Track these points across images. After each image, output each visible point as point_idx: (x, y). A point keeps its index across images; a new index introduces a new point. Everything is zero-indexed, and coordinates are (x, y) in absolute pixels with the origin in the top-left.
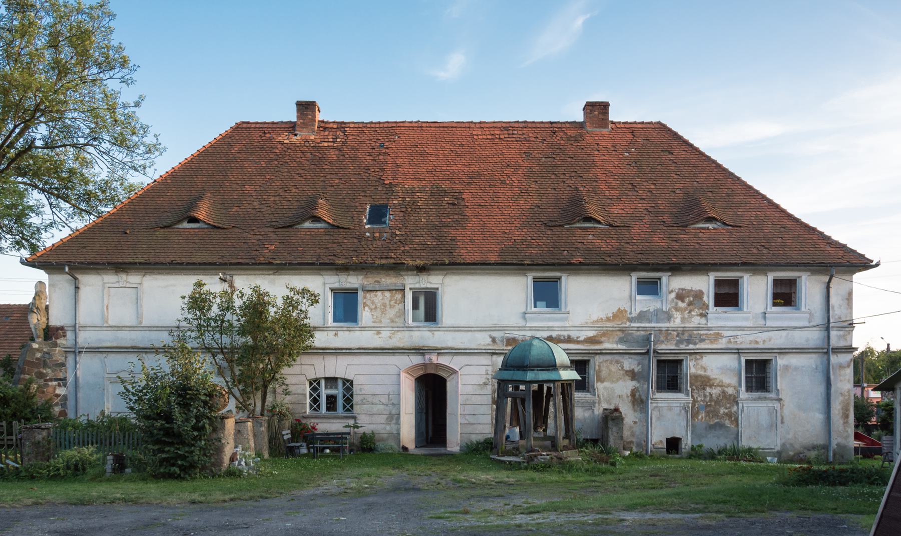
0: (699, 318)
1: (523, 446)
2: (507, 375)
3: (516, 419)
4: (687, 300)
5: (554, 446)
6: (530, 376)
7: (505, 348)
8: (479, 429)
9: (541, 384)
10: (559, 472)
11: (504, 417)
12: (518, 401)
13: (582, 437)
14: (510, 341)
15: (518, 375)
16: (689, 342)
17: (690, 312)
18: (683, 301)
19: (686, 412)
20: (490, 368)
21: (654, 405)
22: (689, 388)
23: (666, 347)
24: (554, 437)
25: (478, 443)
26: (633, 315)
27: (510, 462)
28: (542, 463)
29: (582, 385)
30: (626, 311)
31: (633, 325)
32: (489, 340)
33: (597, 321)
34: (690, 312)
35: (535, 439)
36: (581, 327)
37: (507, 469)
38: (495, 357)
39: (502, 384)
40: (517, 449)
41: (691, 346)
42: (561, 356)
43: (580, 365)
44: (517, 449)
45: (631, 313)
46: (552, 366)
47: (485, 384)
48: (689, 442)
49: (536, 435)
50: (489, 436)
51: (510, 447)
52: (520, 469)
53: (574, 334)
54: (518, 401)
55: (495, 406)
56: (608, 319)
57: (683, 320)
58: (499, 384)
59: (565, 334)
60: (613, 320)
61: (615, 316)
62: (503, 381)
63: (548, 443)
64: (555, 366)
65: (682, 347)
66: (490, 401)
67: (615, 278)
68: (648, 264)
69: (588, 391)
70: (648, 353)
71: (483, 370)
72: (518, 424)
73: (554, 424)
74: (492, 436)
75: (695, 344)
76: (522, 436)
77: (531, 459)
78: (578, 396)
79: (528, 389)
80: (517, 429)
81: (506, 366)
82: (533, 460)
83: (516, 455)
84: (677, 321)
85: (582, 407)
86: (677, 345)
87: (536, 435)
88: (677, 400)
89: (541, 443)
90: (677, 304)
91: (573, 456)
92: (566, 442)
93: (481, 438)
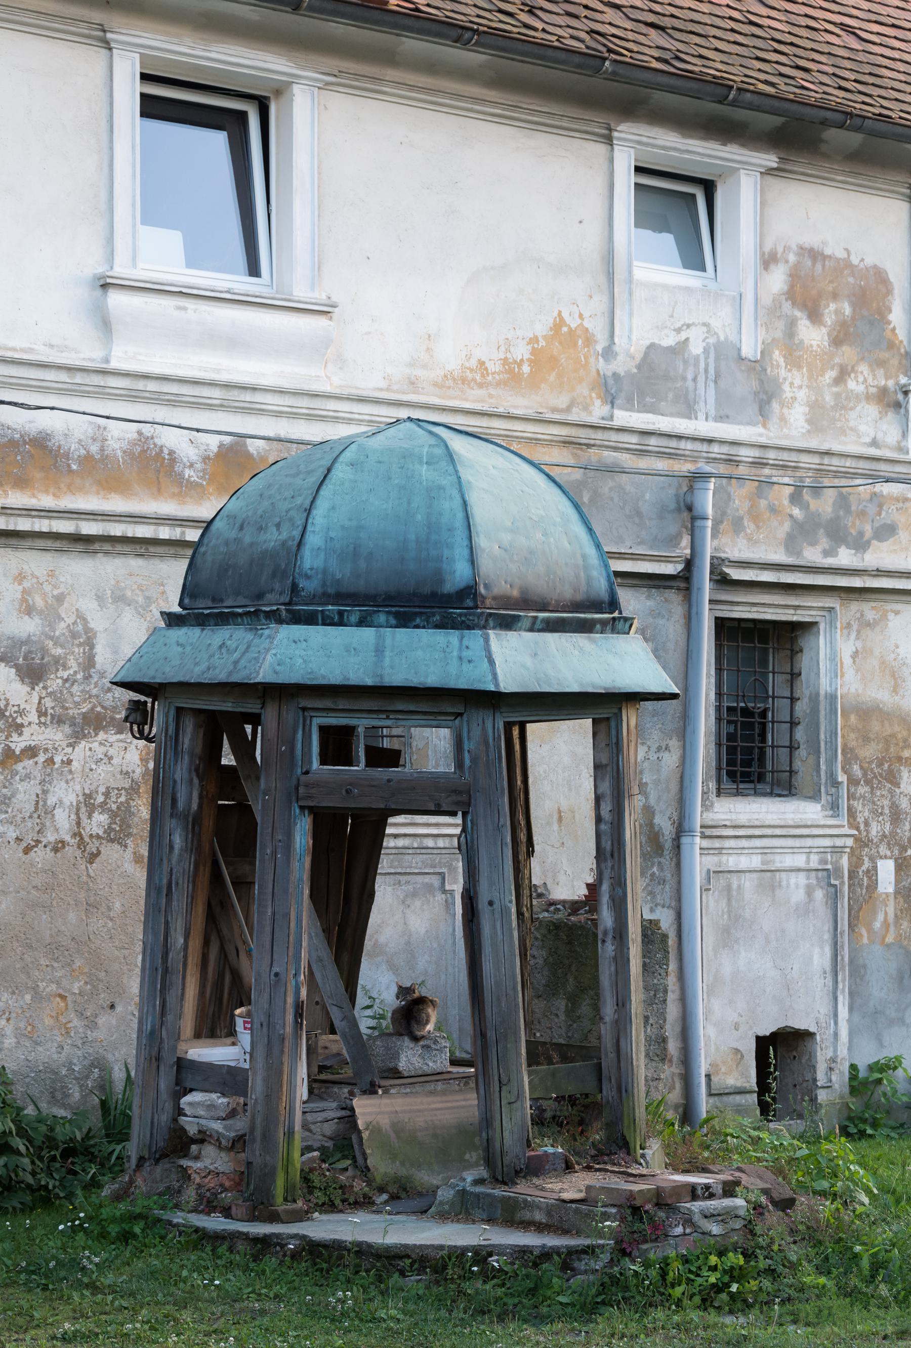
0: (872, 410)
4: (830, 312)
16: (838, 535)
17: (840, 379)
18: (815, 316)
19: (834, 897)
21: (711, 862)
22: (842, 778)
23: (751, 542)
26: (622, 365)
30: (589, 340)
31: (622, 417)
33: (462, 381)
34: (840, 379)
41: (845, 557)
45: (609, 352)
48: (843, 1051)
56: (511, 375)
57: (818, 417)
60: (534, 383)
61: (544, 361)
65: (812, 555)
67: (542, 141)
68: (719, 89)
70: (683, 581)
75: (860, 545)
81: (205, 603)
84: (792, 425)
86: (790, 543)
88: (793, 832)
90: (791, 325)
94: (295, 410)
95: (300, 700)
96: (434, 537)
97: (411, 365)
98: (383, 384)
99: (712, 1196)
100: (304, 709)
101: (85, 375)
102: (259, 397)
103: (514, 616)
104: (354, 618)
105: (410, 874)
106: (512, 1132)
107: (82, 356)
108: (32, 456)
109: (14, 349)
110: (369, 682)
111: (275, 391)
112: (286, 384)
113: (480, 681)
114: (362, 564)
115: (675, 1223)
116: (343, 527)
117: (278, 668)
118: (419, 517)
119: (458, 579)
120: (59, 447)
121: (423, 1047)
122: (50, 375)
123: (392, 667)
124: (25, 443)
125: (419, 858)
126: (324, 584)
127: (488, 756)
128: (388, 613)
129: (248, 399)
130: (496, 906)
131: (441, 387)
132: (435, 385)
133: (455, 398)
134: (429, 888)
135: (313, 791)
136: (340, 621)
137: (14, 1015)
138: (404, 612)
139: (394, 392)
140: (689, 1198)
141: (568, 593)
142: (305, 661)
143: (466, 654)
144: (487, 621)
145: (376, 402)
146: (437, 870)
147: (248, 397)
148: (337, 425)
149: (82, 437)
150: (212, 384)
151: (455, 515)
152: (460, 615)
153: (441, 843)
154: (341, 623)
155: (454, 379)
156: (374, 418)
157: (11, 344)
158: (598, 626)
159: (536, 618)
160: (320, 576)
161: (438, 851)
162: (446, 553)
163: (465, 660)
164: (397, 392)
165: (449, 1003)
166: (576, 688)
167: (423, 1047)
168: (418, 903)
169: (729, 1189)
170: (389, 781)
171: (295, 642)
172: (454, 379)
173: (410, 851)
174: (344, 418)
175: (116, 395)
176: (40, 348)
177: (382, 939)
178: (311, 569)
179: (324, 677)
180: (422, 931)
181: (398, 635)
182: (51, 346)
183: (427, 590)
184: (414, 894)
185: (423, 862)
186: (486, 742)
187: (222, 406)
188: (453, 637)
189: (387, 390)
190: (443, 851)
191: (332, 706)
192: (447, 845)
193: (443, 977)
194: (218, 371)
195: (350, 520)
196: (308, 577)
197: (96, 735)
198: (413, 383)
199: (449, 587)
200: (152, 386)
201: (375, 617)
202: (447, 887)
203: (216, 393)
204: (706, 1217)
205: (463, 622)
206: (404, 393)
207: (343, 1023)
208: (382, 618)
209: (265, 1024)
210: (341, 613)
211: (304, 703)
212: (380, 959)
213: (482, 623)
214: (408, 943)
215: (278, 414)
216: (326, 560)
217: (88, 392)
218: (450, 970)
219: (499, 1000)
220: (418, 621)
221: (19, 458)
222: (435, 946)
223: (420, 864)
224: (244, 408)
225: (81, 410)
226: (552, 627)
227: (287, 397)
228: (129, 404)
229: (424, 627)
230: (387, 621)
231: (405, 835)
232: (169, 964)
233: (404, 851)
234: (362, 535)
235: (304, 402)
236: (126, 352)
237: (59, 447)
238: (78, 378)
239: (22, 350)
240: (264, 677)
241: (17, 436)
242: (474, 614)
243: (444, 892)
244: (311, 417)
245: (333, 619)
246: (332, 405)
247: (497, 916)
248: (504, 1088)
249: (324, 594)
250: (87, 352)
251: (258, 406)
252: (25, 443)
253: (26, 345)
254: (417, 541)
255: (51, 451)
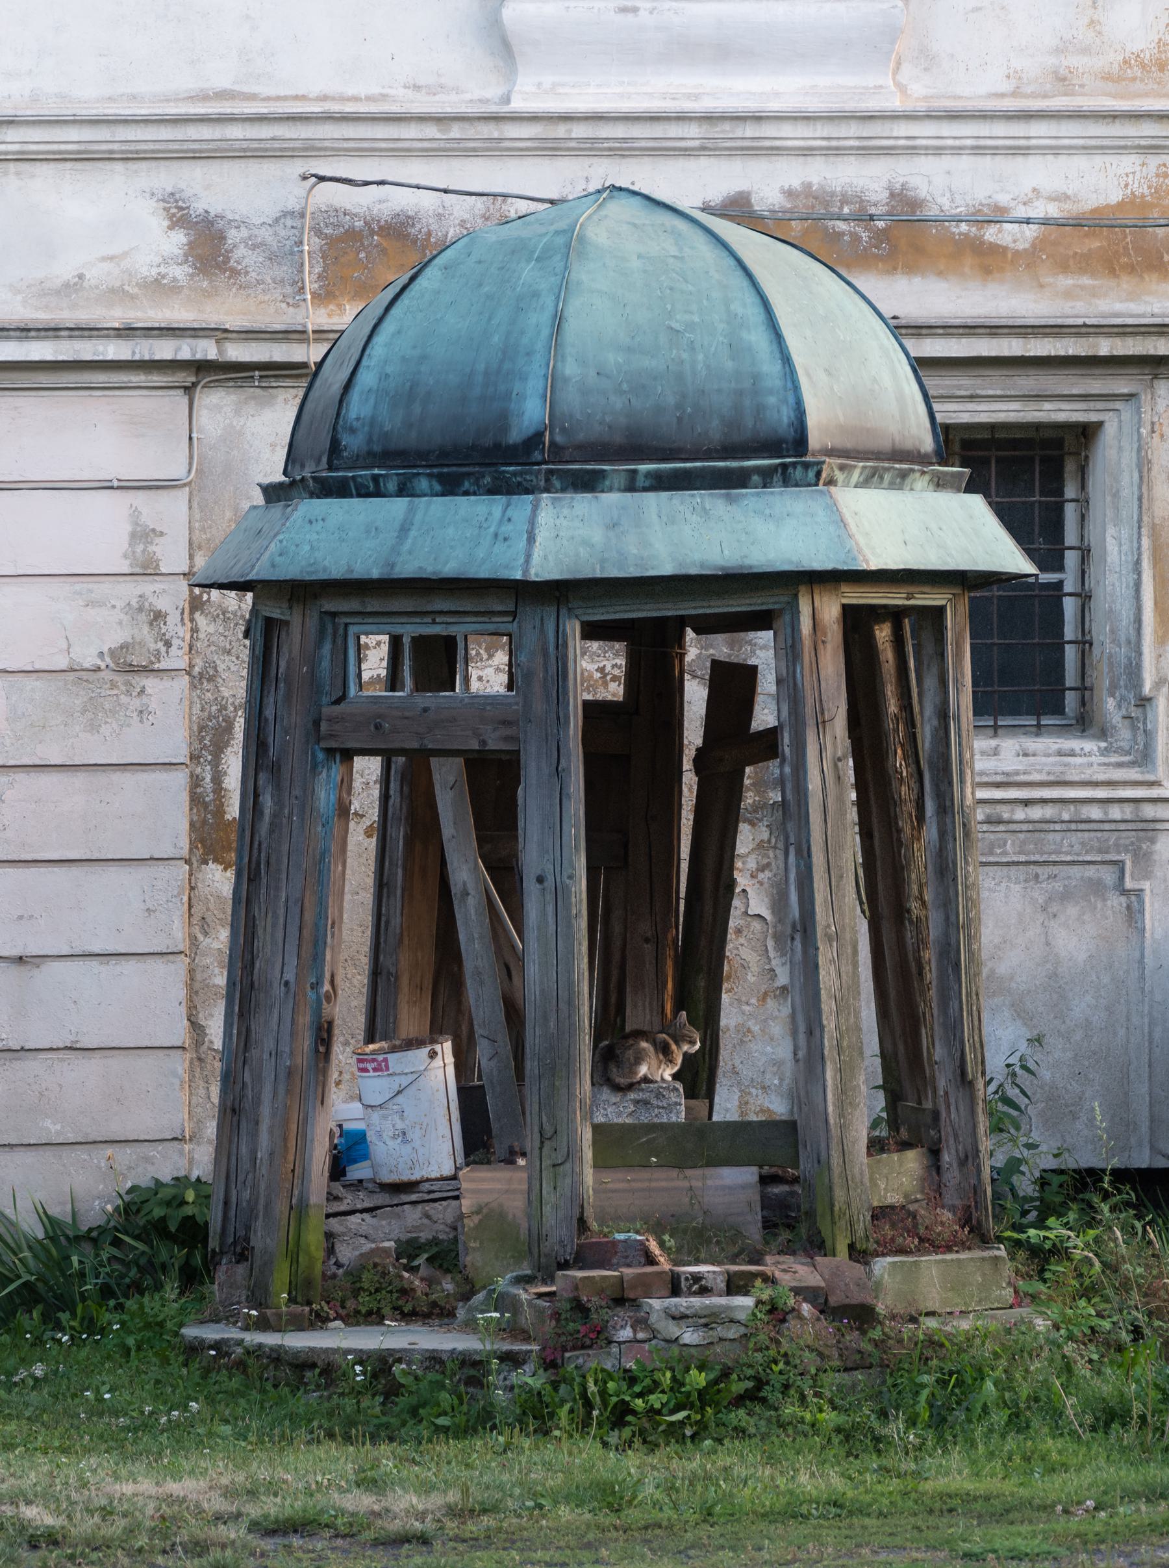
1: (493, 1220)
2: (346, 536)
3: (430, 973)
5: (792, 1213)
6: (562, 535)
7: (318, 318)
8: (77, 1095)
9: (649, 617)
10: (852, 1440)
11: (315, 946)
12: (447, 778)
13: (1044, 1148)
14: (381, 255)
15: (456, 534)
20: (171, 513)
24: (789, 1129)
25: (61, 1236)
27: (381, 1365)
28: (686, 1359)
29: (1029, 649)
32: (160, 247)
35: (614, 1145)
36: (1013, 123)
37: (344, 1431)
38: (218, 407)
39: (300, 626)
40: (444, 1255)
42: (849, 360)
43: (1027, 472)
44: (444, 1255)
46: (772, 452)
47: (130, 666)
49: (616, 1111)
50: (166, 1166)
51: (369, 1236)
52: (483, 1421)
53: (948, 184)
54: (447, 778)
55: (220, 880)
58: (265, 635)
59: (871, 180)
62: (301, 592)
63: (732, 1185)
64: (800, 442)
66: (173, 828)
69: (1085, 722)
71: (98, 532)
72: (448, 1017)
73: (780, 1029)
74: (201, 1161)
76: (479, 1137)
77: (580, 1323)
78: (1000, 761)
79: (539, 677)
80: (437, 1070)
81: (327, 465)
82: (600, 1337)
83: (437, 1313)
85: (1032, 866)
87: (616, 1111)
89: (665, 1187)
91: (948, 1293)
92: (899, 1177)
93: (88, 1189)
94: (834, 143)
95: (324, 602)
96: (507, 366)
97: (1059, 51)
98: (1006, 87)
99: (704, 1291)
100: (334, 615)
101: (466, 125)
102: (768, 130)
103: (594, 471)
104: (392, 486)
105: (1055, 863)
106: (556, 1207)
107: (468, 96)
108: (384, 251)
109: (356, 99)
110: (375, 574)
111: (795, 118)
112: (813, 105)
113: (506, 567)
114: (417, 409)
115: (621, 1323)
116: (404, 359)
117: (278, 559)
118: (496, 339)
119: (526, 423)
120: (429, 234)
121: (637, 1102)
122: (411, 131)
123: (410, 553)
124: (372, 232)
125: (1074, 838)
126: (370, 441)
127: (546, 671)
128: (430, 475)
129: (749, 134)
130: (549, 883)
131: (1119, 80)
132: (1107, 77)
133: (1146, 95)
134: (1096, 887)
135: (336, 727)
136: (374, 491)
137: (346, 1077)
138: (448, 474)
139: (1026, 96)
140: (667, 1292)
141: (715, 431)
142: (312, 548)
143: (506, 529)
144: (547, 480)
145: (984, 117)
146: (1108, 857)
147: (750, 130)
148: (916, 159)
149: (466, 216)
150: (681, 118)
151: (539, 333)
152: (515, 474)
153: (1115, 812)
154: (378, 494)
155: (1143, 65)
156: (982, 142)
157: (350, 91)
158: (756, 478)
159: (635, 471)
160: (366, 428)
161: (1113, 826)
162: (517, 387)
163: (501, 538)
164: (1033, 96)
165: (1132, 1076)
166: (667, 569)
167: (637, 1102)
168: (1072, 911)
169: (735, 1286)
170: (425, 710)
171: (310, 522)
172: (1143, 65)
173: (1058, 827)
174: (927, 148)
175: (521, 149)
176: (400, 92)
177: (1002, 969)
178: (358, 419)
179: (325, 569)
180: (1082, 957)
181: (433, 507)
182: (417, 88)
183: (488, 441)
184: (1066, 896)
185: (1083, 844)
186: (545, 654)
187: (703, 148)
188: (495, 506)
189: (1015, 94)
190: (1123, 826)
191: (360, 609)
192: (1128, 816)
193: (1122, 1032)
194: (697, 97)
195: (414, 347)
196: (353, 431)
197: (491, 656)
198: (1064, 79)
199: (515, 436)
200: (580, 131)
201: (415, 481)
202: (1129, 884)
203: (693, 131)
204: (674, 1318)
205: (519, 484)
206: (1045, 96)
207: (493, 1063)
208: (423, 484)
209: (274, 1053)
210: (375, 478)
211: (330, 606)
212: (998, 1000)
213: (542, 483)
214: (1054, 976)
215: (806, 152)
216: (375, 407)
217: (474, 150)
218: (1135, 1020)
219: (546, 1018)
220: (466, 485)
221: (362, 255)
222: (1106, 980)
223: (1077, 848)
224: (742, 149)
225: (414, 182)
226: (661, 483)
227: (819, 125)
228: (546, 162)
229: (475, 494)
230: (431, 487)
231: (1044, 801)
232: (255, 977)
233: (1045, 826)
234: (423, 368)
235: (853, 129)
236: (539, 85)
237: (429, 234)
238: (456, 131)
239: (369, 99)
240: (257, 574)
241: (359, 224)
242: (531, 473)
243: (1124, 892)
244: (866, 151)
245: (368, 488)
246: (902, 129)
247: (550, 897)
248: (547, 1144)
249: (370, 454)
250: (475, 89)
251: (767, 143)
252: (372, 232)
253: (376, 90)
254: (486, 373)
255: (415, 242)
